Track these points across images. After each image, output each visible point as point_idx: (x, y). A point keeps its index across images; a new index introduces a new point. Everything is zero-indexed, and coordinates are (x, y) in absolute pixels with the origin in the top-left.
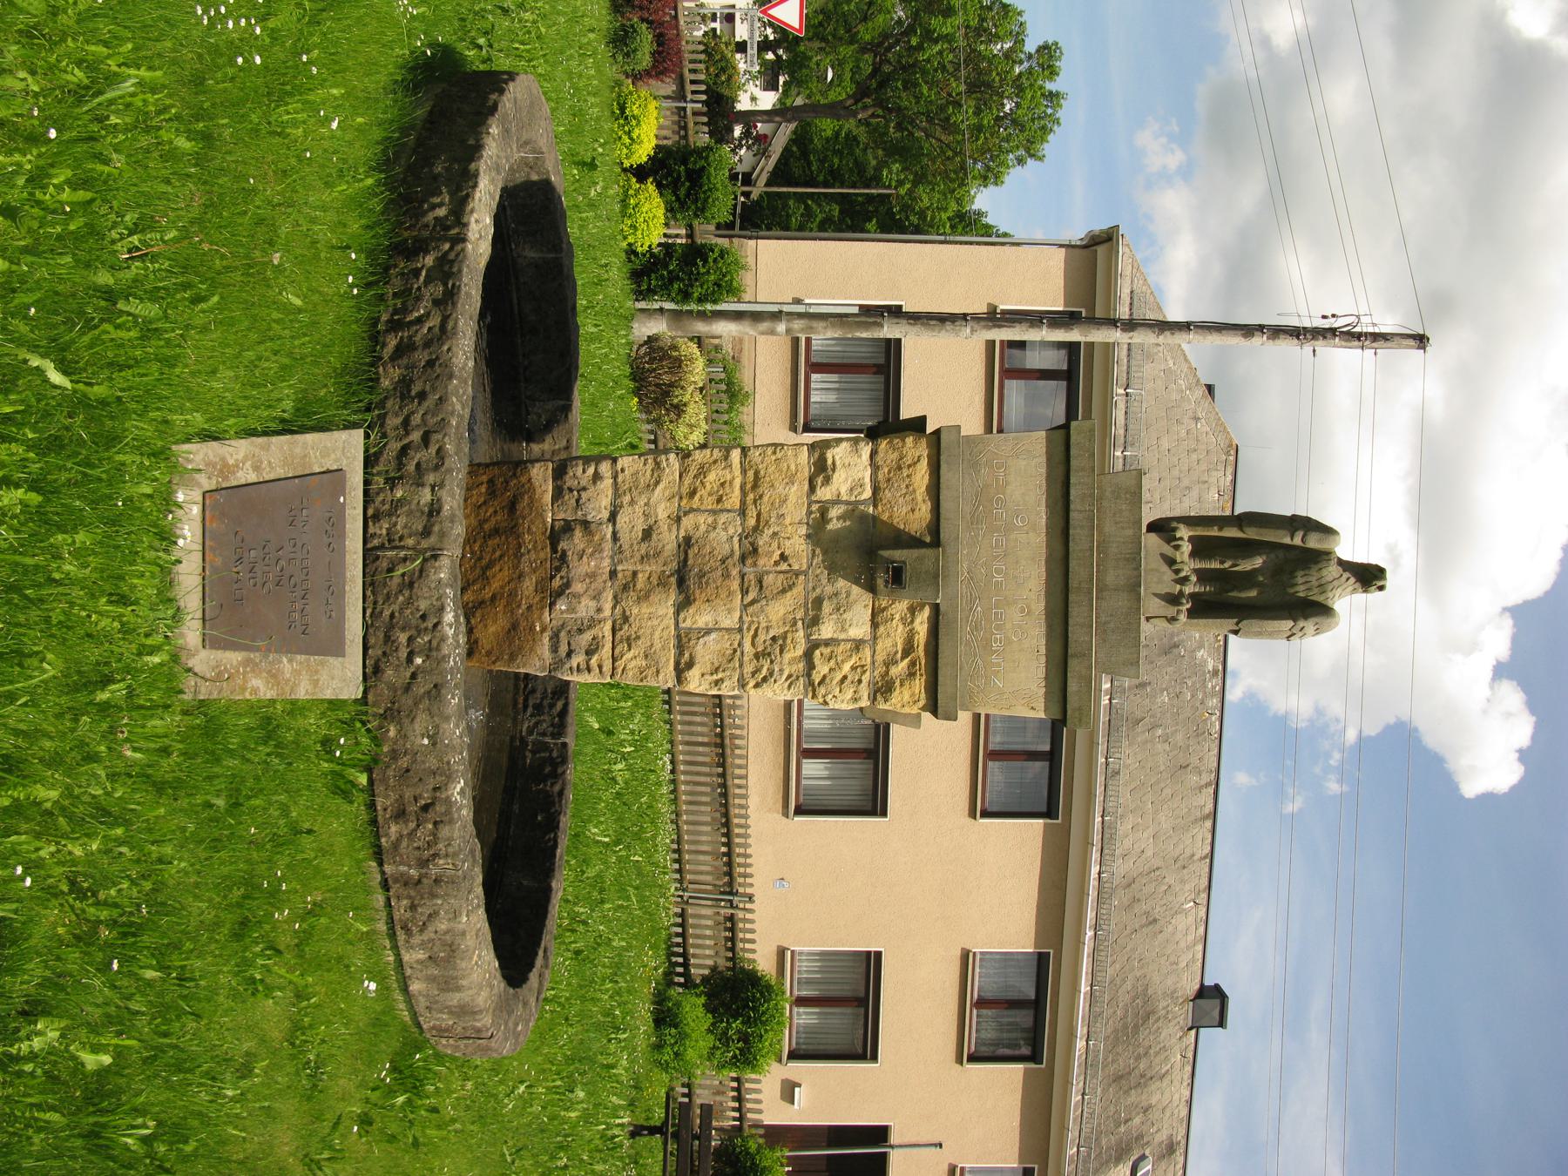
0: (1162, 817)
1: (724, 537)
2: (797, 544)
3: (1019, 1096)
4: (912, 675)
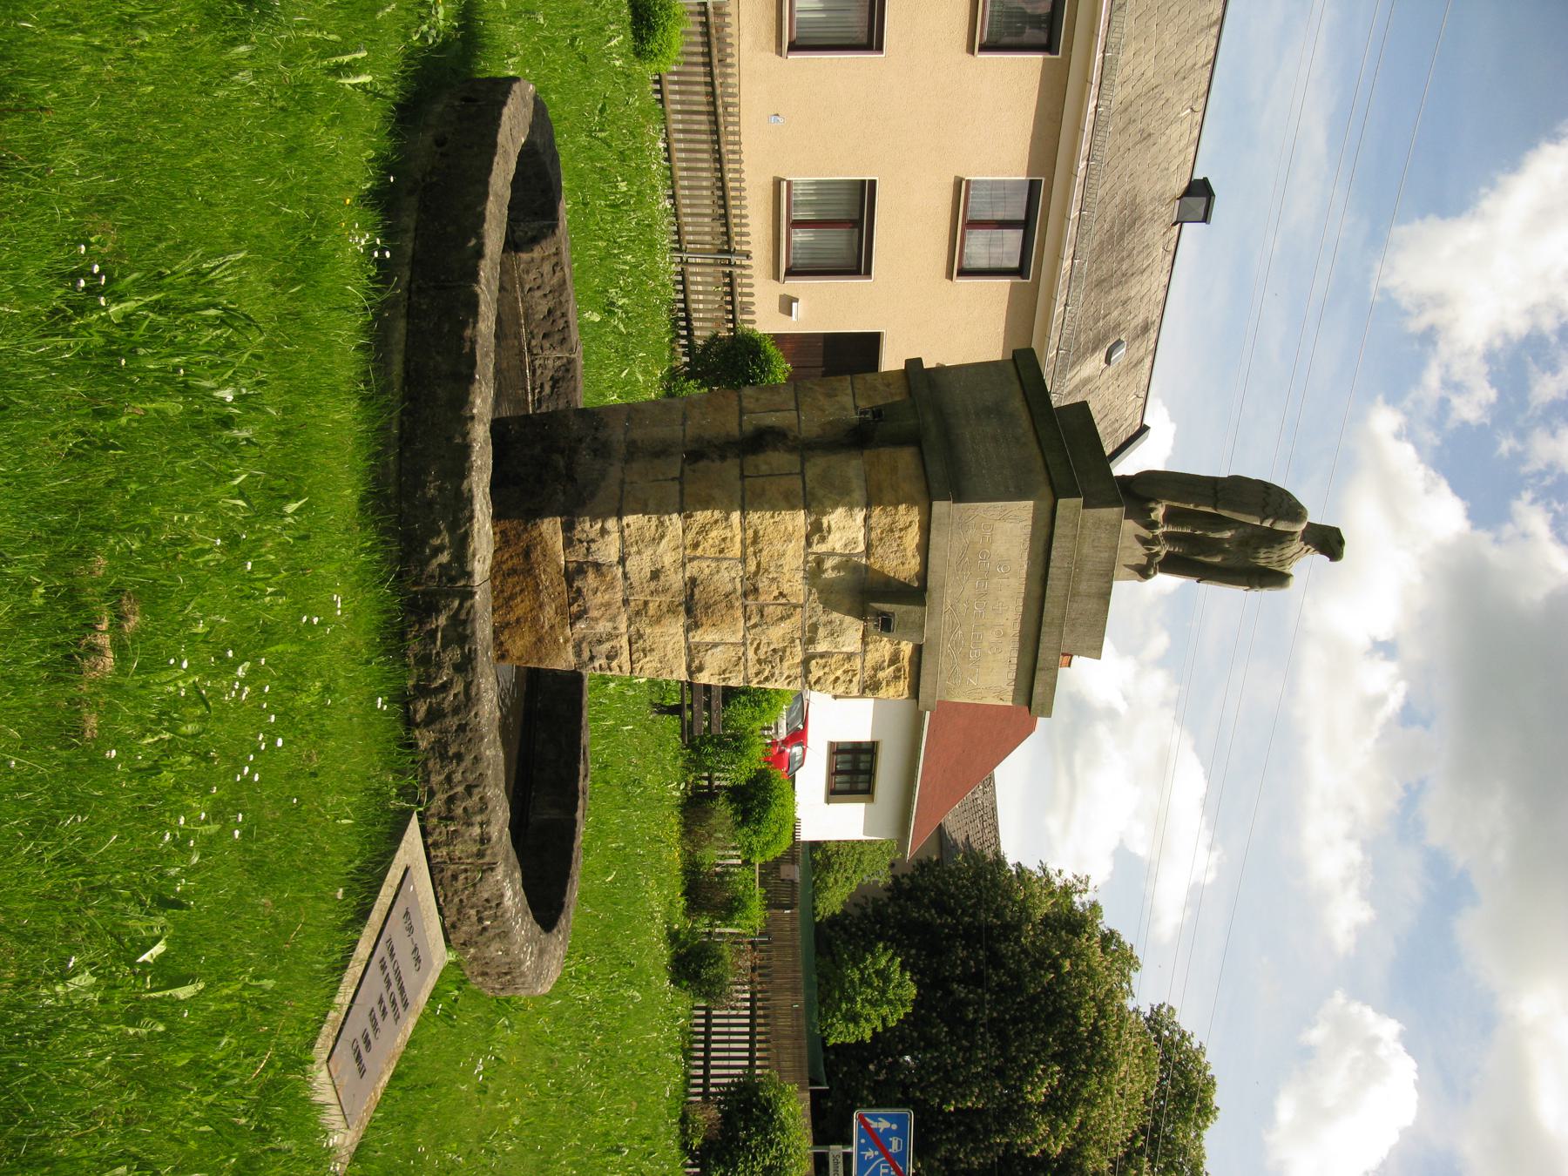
0: (1166, 36)
1: (728, 577)
2: (796, 586)
3: (1005, 305)
4: (897, 678)
